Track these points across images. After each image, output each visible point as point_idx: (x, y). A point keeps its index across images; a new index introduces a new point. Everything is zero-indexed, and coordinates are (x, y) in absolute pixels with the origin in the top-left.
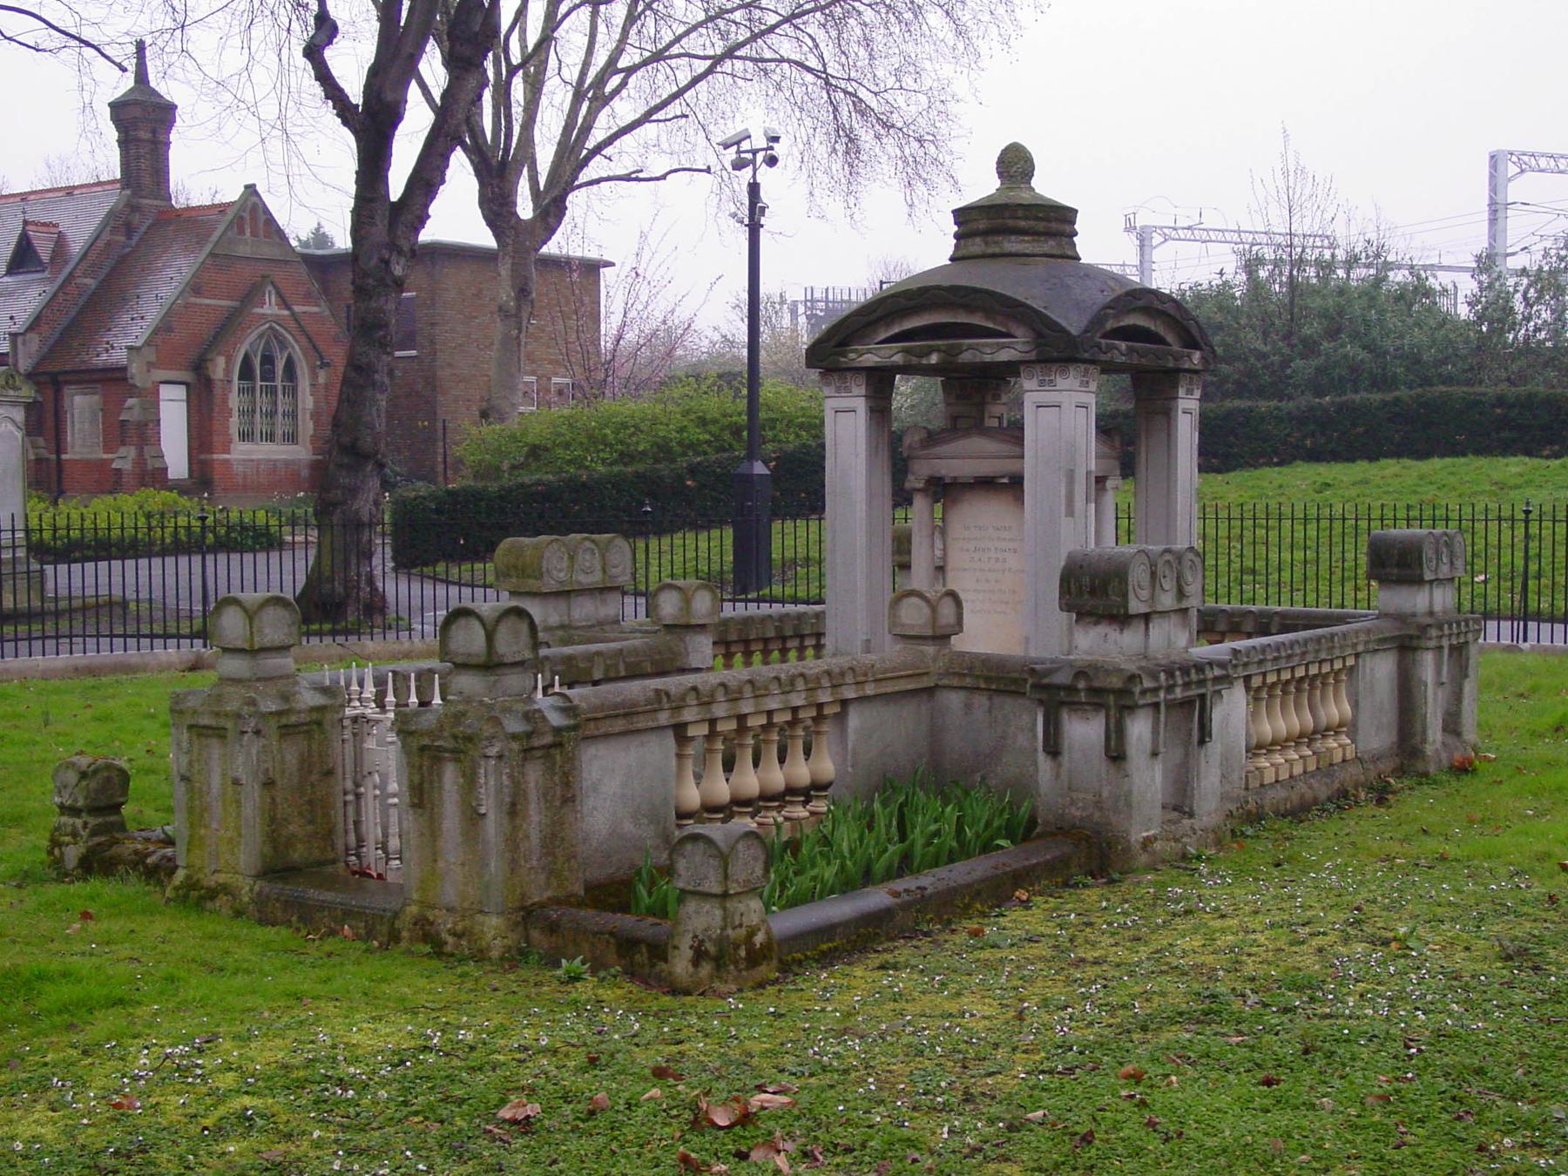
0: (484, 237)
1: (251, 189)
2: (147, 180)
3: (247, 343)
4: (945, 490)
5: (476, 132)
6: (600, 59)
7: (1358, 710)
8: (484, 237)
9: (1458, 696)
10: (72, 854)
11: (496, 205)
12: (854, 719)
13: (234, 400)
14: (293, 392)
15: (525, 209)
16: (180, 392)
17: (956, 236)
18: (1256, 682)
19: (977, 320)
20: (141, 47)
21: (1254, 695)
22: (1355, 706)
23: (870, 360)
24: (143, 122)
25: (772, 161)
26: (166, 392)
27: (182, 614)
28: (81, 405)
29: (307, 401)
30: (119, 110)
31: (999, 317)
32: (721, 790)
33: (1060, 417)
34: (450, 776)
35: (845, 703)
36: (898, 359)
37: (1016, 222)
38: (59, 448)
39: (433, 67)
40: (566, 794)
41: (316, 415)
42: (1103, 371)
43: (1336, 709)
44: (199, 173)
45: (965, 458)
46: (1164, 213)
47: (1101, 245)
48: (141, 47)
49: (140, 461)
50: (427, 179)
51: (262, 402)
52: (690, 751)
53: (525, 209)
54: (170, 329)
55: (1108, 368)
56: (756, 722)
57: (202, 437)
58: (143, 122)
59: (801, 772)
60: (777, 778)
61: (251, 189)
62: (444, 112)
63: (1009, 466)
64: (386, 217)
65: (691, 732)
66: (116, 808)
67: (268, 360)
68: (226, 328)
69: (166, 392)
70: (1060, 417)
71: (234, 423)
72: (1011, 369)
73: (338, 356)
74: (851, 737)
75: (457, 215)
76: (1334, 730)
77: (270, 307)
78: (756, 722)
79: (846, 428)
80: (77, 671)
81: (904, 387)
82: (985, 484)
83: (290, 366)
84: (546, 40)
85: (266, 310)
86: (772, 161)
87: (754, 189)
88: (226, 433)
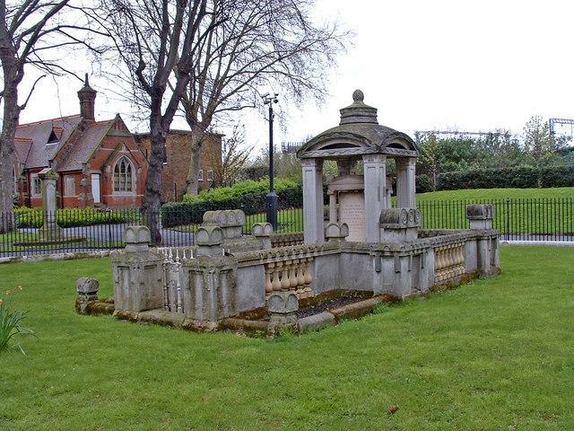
0: (187, 128)
1: (118, 115)
2: (88, 114)
3: (117, 161)
4: (340, 195)
5: (185, 98)
6: (222, 74)
7: (465, 258)
8: (187, 128)
9: (494, 254)
10: (83, 306)
11: (191, 119)
12: (317, 263)
13: (113, 179)
14: (130, 176)
15: (200, 119)
16: (98, 176)
17: (341, 118)
18: (437, 249)
19: (349, 142)
20: (87, 75)
21: (436, 253)
22: (465, 257)
23: (316, 155)
24: (87, 96)
25: (276, 101)
26: (93, 176)
27: (116, 229)
28: (69, 181)
29: (134, 178)
30: (80, 94)
31: (357, 141)
32: (278, 283)
33: (374, 171)
34: (198, 279)
35: (314, 257)
36: (327, 155)
37: (359, 112)
38: (62, 195)
39: (173, 79)
40: (234, 286)
41: (137, 183)
42: (387, 158)
43: (460, 258)
44: (103, 111)
45: (347, 183)
46: (404, 114)
47: (383, 120)
48: (87, 75)
49: (86, 197)
50: (172, 109)
51: (121, 179)
52: (269, 272)
53: (200, 119)
54: (94, 158)
55: (389, 157)
56: (288, 263)
57: (104, 190)
58: (87, 96)
59: (302, 279)
60: (295, 280)
61: (118, 115)
62: (176, 92)
63: (359, 187)
64: (160, 121)
65: (269, 266)
66: (95, 293)
67: (123, 166)
68: (111, 157)
69: (93, 176)
70: (374, 171)
71: (113, 186)
72: (360, 157)
73: (146, 165)
74: (316, 269)
75: (179, 123)
76: (459, 264)
77: (124, 150)
78: (288, 263)
79: (309, 175)
80: (66, 259)
81: (327, 163)
82: (351, 192)
83: (129, 168)
84: (206, 68)
85: (122, 151)
86: (276, 101)
87: (271, 110)
88: (111, 188)
